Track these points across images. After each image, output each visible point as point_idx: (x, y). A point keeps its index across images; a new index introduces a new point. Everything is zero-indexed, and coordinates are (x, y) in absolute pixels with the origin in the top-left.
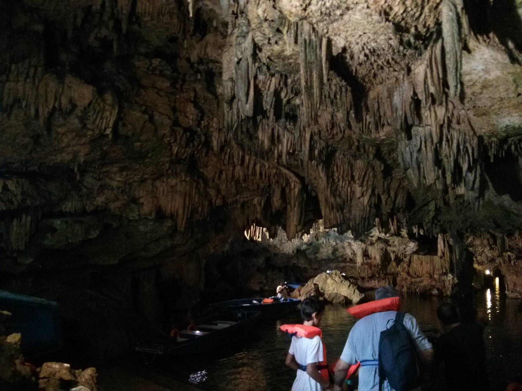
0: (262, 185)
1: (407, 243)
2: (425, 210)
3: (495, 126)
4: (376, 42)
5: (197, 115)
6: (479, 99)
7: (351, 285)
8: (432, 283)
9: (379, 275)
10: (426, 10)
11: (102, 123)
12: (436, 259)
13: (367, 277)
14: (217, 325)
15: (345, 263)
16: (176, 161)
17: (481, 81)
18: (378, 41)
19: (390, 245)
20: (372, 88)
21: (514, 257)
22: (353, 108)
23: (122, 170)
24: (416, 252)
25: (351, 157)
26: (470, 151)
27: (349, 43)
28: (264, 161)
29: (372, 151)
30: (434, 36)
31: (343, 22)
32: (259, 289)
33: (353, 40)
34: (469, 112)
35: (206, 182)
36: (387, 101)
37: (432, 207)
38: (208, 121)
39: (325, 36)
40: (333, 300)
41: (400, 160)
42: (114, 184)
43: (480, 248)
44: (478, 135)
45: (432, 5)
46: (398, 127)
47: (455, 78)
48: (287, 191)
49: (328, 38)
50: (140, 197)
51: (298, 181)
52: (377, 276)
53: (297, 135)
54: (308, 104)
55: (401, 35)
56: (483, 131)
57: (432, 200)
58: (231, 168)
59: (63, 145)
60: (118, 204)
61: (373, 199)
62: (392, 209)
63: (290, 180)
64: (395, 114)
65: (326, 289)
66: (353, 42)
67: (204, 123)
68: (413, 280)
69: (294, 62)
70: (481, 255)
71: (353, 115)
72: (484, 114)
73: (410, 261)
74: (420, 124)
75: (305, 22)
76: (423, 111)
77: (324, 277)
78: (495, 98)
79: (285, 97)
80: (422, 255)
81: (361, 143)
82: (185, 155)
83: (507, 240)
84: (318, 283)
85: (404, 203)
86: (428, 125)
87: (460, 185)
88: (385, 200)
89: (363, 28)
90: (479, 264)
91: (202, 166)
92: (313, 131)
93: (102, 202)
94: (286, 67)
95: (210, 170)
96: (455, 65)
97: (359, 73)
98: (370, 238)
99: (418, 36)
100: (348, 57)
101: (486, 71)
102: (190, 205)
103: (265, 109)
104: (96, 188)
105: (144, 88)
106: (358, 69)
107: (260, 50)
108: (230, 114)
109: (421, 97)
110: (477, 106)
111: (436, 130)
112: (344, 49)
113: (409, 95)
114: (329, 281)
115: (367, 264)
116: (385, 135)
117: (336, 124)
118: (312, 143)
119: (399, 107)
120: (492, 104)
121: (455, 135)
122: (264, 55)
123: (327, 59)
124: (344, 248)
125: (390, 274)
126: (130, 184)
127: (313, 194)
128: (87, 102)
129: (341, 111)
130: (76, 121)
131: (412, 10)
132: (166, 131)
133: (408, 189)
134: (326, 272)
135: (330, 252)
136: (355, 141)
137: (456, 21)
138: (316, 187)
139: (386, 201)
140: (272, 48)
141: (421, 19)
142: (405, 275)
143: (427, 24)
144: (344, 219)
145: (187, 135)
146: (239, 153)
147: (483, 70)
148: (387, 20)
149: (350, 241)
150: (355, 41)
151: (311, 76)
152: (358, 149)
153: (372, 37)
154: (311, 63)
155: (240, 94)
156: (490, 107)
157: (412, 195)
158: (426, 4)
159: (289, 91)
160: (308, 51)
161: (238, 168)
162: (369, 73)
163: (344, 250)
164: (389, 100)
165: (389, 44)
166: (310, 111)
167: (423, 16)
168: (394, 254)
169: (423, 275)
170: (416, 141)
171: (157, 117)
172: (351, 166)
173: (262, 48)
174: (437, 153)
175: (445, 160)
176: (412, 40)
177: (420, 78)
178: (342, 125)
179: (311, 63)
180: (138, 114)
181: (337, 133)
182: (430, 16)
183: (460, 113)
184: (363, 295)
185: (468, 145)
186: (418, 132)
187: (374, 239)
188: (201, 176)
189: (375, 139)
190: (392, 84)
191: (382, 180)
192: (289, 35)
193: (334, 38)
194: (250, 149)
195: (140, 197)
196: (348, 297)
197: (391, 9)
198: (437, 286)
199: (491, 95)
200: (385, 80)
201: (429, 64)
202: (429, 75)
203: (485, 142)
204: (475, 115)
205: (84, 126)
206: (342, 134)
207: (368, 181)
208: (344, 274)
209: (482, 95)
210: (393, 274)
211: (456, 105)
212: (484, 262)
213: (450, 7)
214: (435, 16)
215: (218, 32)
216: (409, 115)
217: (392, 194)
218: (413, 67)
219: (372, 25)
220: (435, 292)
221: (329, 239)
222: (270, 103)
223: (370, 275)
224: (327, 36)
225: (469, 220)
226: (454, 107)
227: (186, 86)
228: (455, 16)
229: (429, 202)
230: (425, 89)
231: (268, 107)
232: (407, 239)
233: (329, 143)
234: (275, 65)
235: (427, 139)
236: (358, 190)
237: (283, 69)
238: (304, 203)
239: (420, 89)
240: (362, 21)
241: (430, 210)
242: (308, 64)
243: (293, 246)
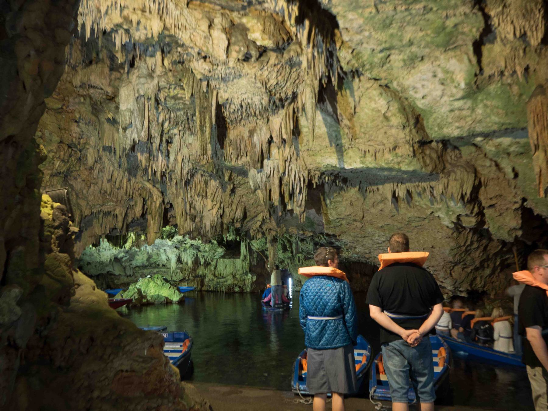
10: (288, 84)
12: (239, 262)
18: (254, 99)
21: (303, 257)
24: (223, 257)
56: (312, 166)
65: (149, 292)
66: (236, 97)
68: (219, 280)
83: (300, 243)
98: (184, 245)
99: (281, 100)
135: (145, 259)
141: (284, 89)
159: (172, 122)
167: (286, 87)
169: (227, 276)
172: (206, 183)
174: (281, 179)
177: (277, 128)
184: (182, 295)
185: (301, 176)
187: (187, 246)
196: (169, 297)
199: (320, 143)
202: (283, 126)
204: (307, 155)
215: (105, 64)
217: (234, 207)
218: (271, 118)
220: (237, 289)
223: (181, 278)
232: (217, 245)
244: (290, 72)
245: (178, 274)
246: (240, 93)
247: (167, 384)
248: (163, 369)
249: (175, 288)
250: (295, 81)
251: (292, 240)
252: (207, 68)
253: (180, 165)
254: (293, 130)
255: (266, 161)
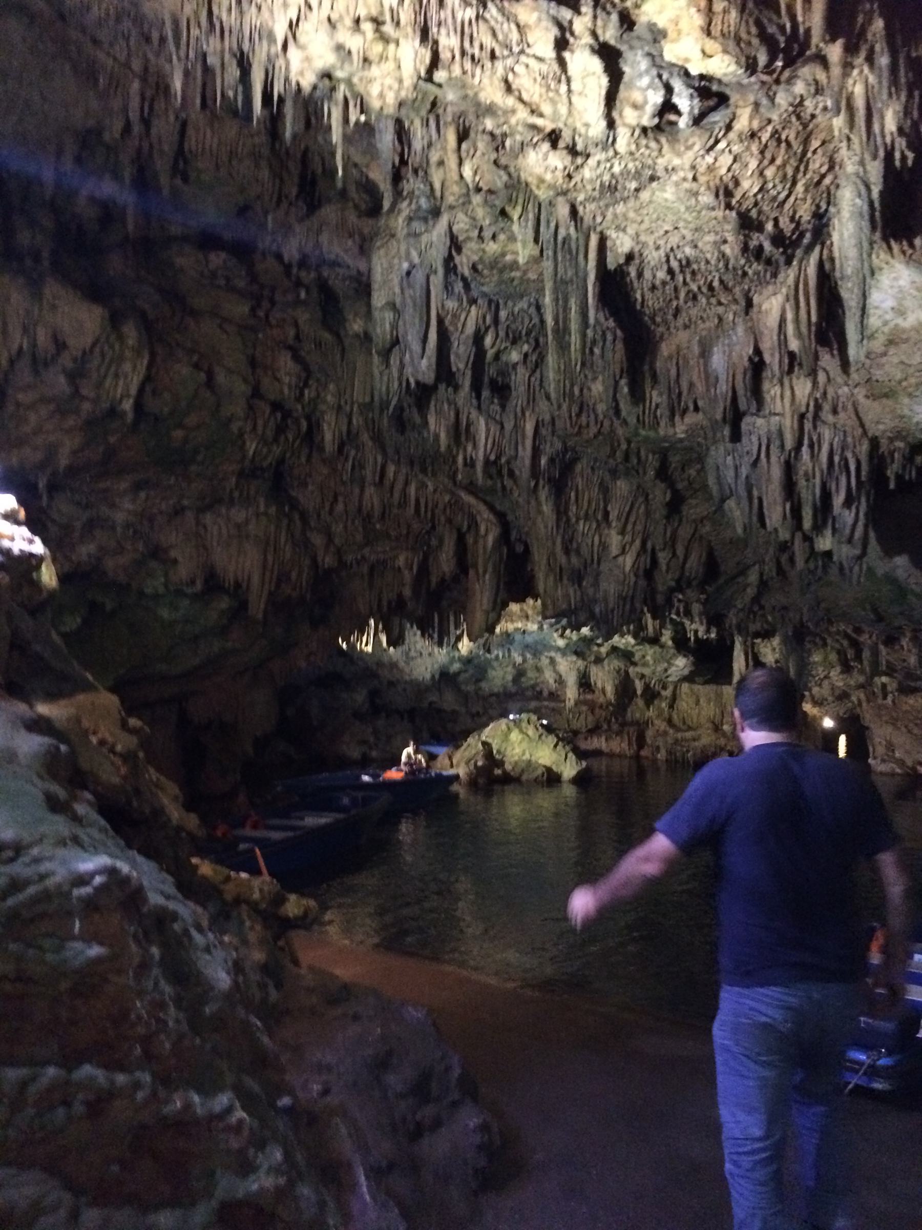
0: (416, 526)
1: (671, 658)
2: (738, 583)
3: (905, 420)
4: (696, 247)
5: (299, 377)
6: (880, 366)
7: (560, 743)
8: (718, 742)
9: (609, 726)
10: (800, 188)
11: (116, 385)
12: (729, 691)
13: (584, 730)
14: (302, 819)
15: (541, 701)
16: (251, 472)
17: (886, 329)
18: (700, 244)
19: (635, 664)
20: (666, 336)
22: (624, 375)
23: (137, 487)
24: (689, 679)
25: (607, 473)
26: (853, 467)
27: (640, 246)
28: (427, 475)
29: (653, 461)
30: (807, 239)
31: (638, 203)
32: (359, 757)
33: (650, 240)
34: (856, 391)
35: (304, 517)
36: (698, 363)
37: (753, 577)
38: (317, 390)
39: (595, 230)
40: (521, 775)
41: (711, 481)
42: (120, 517)
43: (820, 669)
44: (870, 435)
45: (812, 179)
46: (719, 416)
47: (859, 326)
48: (470, 540)
49: (601, 233)
50: (171, 547)
51: (494, 521)
52: (605, 727)
53: (509, 426)
54: (559, 364)
55: (745, 236)
56: (881, 427)
57: (754, 565)
58: (357, 491)
59: (27, 429)
60: (123, 560)
61: (643, 559)
62: (678, 581)
63: (479, 518)
64: (713, 390)
65: (508, 753)
67: (309, 394)
68: (679, 735)
69: (521, 278)
70: (820, 685)
71: (626, 390)
72: (886, 396)
73: (674, 698)
74: (759, 410)
75: (560, 199)
76: (766, 386)
77: (504, 727)
78: (910, 366)
79: (492, 347)
80: (699, 684)
81: (632, 445)
82: (269, 459)
84: (490, 740)
85: (701, 570)
86: (775, 414)
87: (822, 532)
88: (665, 562)
89: (675, 218)
90: (817, 703)
91: (296, 483)
92: (540, 419)
93: (89, 555)
94: (503, 286)
95: (312, 492)
96: (862, 303)
97: (648, 306)
98: (595, 648)
99: (778, 239)
100: (633, 274)
101: (900, 311)
102: (276, 566)
103: (454, 369)
104: (78, 525)
105: (194, 313)
106: (646, 298)
107: (459, 250)
108: (385, 378)
109: (772, 359)
110: (874, 378)
111: (793, 422)
112: (630, 257)
113: (744, 354)
114: (515, 736)
115: (585, 702)
116: (687, 432)
117: (588, 406)
118: (537, 443)
119: (723, 377)
120: (904, 376)
121: (827, 434)
122: (465, 260)
123: (598, 277)
124: (538, 669)
125: (633, 723)
126: (151, 520)
127: (520, 548)
128: (89, 340)
129: (600, 378)
130: (62, 379)
131: (774, 186)
132: (238, 408)
133: (710, 542)
134: (507, 717)
135: (509, 678)
136: (623, 441)
137: (867, 217)
138: (527, 534)
139: (668, 565)
140: (483, 246)
141: (787, 206)
142: (662, 725)
143: (797, 217)
144: (582, 600)
145: (276, 418)
146: (376, 458)
147: (893, 309)
148: (729, 206)
149: (553, 654)
150: (655, 243)
151: (566, 309)
152: (627, 458)
153: (689, 237)
154: (567, 283)
155: (410, 338)
156: (900, 382)
157: (716, 553)
158: (800, 175)
159: (502, 334)
160: (560, 259)
161: (370, 491)
162: (667, 307)
163: (537, 675)
164: (701, 361)
165: (720, 252)
166: (562, 377)
167: (792, 199)
168: (643, 681)
170: (750, 443)
171: (221, 378)
172: (605, 490)
173: (463, 245)
174: (789, 468)
175: (802, 483)
176: (767, 246)
177: (772, 321)
178: (601, 408)
179: (567, 283)
180: (186, 371)
181: (588, 425)
182: (805, 199)
183: (840, 392)
184: (584, 764)
185: (849, 455)
186: (754, 427)
188: (294, 505)
189: (665, 439)
190: (709, 330)
191: (664, 521)
192: (523, 224)
193: (612, 233)
194: (398, 452)
195: (171, 547)
196: (554, 768)
197: (737, 183)
198: (729, 748)
199: (903, 358)
200: (695, 323)
201: (792, 292)
202: (790, 316)
203: (881, 450)
204: (867, 397)
205: (76, 393)
206: (599, 426)
207: (635, 524)
208: (545, 722)
209: (884, 360)
210: (637, 723)
211: (832, 376)
212: (826, 700)
213: (857, 188)
214: (814, 200)
216: (741, 392)
217: (680, 551)
218: (756, 299)
219: (694, 214)
221: (509, 650)
222: (464, 358)
223: (590, 727)
224: (599, 229)
225: (823, 605)
226: (829, 380)
227: (276, 315)
228: (866, 208)
229: (748, 567)
230: (780, 345)
231: (461, 366)
232: (672, 651)
233: (569, 444)
234: (482, 280)
235: (772, 440)
236: (615, 540)
237: (497, 290)
238: (502, 566)
239: (768, 344)
240: (675, 205)
241: (748, 585)
242: (561, 285)
243: (433, 665)
244: (804, 153)
245: (583, 716)
246: (662, 232)
247: (141, 1030)
248: (132, 983)
249: (568, 748)
250: (823, 176)
251: (861, 639)
252: (560, 166)
253: (529, 443)
254: (819, 325)
255: (746, 424)
